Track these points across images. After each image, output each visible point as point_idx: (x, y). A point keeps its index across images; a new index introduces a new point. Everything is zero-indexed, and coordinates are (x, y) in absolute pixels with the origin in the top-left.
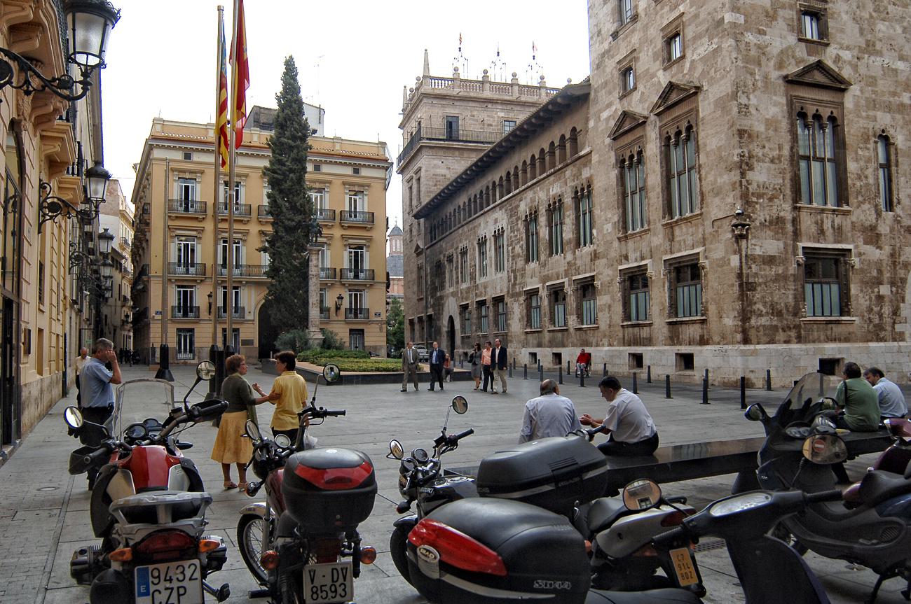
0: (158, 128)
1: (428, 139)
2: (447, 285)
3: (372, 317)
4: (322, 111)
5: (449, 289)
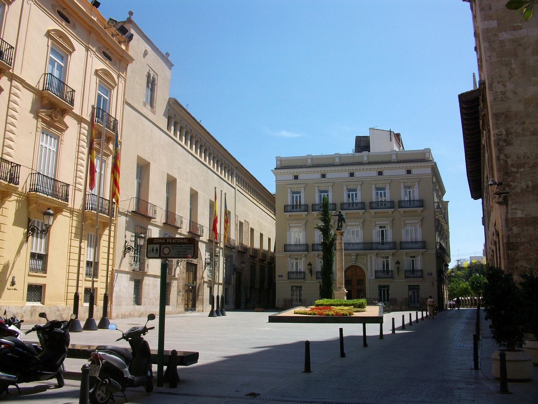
4: (392, 133)
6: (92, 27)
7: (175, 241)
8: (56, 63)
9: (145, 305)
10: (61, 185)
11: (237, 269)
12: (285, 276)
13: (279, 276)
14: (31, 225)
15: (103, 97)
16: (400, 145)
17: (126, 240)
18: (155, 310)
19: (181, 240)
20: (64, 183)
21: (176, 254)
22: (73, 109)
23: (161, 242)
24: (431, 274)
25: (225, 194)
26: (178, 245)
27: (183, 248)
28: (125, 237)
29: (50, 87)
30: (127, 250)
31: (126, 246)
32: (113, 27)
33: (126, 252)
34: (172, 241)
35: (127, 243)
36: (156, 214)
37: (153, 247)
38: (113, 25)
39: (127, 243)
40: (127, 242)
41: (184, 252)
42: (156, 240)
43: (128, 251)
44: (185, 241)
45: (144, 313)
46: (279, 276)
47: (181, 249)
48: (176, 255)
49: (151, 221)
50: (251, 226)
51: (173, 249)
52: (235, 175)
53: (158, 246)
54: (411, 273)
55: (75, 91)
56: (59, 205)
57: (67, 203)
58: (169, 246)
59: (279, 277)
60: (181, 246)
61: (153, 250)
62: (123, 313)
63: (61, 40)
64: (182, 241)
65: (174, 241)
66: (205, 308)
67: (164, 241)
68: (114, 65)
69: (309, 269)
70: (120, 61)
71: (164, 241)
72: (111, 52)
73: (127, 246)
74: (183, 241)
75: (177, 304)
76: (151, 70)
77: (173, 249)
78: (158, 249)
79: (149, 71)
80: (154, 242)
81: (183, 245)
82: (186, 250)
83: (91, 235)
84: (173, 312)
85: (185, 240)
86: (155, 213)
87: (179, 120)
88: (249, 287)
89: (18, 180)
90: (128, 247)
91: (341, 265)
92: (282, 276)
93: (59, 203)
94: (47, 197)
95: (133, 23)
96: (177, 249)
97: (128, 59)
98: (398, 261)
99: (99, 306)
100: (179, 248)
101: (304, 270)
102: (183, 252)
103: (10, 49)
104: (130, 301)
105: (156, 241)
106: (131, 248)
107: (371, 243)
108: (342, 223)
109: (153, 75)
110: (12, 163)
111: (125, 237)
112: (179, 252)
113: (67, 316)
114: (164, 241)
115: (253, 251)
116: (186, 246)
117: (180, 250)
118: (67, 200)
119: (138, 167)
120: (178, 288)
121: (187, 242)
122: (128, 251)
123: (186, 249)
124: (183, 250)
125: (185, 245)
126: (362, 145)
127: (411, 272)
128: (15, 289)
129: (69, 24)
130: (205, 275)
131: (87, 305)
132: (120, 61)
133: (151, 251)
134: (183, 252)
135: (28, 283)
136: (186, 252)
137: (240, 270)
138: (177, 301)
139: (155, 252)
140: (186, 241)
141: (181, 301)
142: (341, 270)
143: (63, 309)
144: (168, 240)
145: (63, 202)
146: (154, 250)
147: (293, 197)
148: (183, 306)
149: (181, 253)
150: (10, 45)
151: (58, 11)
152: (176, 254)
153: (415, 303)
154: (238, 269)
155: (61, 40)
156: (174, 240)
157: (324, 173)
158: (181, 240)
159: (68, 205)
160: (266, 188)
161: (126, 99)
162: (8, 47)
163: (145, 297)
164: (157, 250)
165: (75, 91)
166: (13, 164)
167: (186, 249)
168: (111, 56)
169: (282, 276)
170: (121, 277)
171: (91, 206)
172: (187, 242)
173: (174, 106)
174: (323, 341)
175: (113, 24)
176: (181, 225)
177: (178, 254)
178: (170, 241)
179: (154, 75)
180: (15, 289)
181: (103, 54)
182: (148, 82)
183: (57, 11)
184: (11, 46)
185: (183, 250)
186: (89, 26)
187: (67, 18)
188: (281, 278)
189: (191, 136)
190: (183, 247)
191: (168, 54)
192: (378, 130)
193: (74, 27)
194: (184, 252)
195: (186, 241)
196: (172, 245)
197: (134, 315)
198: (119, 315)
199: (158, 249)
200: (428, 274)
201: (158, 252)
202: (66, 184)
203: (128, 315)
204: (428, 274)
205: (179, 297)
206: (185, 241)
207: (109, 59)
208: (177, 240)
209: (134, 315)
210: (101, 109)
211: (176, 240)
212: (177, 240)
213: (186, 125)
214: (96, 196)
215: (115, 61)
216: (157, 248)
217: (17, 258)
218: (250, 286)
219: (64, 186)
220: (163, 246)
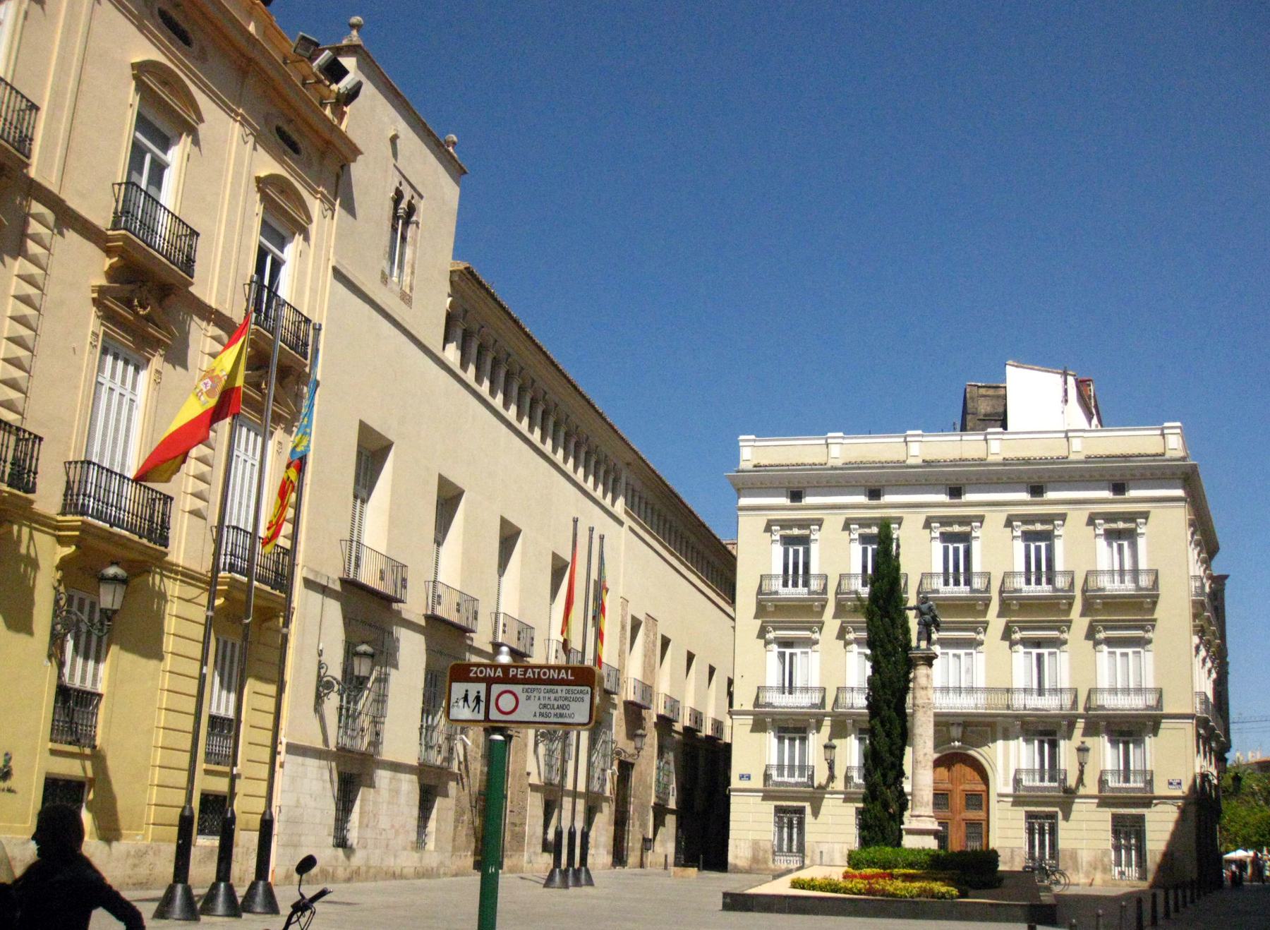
3: (1160, 789)
6: (250, 60)
7: (534, 673)
8: (148, 158)
9: (365, 847)
10: (150, 496)
12: (757, 782)
13: (742, 777)
15: (274, 253)
16: (1091, 413)
17: (320, 661)
18: (392, 865)
19: (552, 671)
20: (157, 492)
21: (538, 715)
22: (191, 284)
23: (492, 675)
24: (1179, 784)
25: (602, 538)
26: (543, 687)
27: (560, 694)
29: (132, 219)
32: (306, 60)
34: (525, 674)
36: (405, 587)
37: (467, 691)
38: (308, 54)
41: (561, 707)
42: (475, 669)
44: (565, 676)
45: (363, 869)
46: (742, 777)
47: (552, 698)
48: (535, 716)
50: (662, 629)
51: (528, 698)
52: (623, 486)
53: (482, 687)
54: (1121, 779)
55: (198, 235)
56: (141, 553)
57: (162, 548)
58: (517, 689)
60: (551, 691)
61: (466, 699)
63: (167, 93)
64: (556, 676)
65: (529, 674)
66: (530, 862)
67: (499, 673)
68: (307, 166)
69: (826, 760)
70: (323, 155)
71: (501, 675)
72: (298, 130)
74: (495, 673)
75: (454, 847)
76: (404, 183)
77: (528, 698)
78: (483, 697)
79: (398, 185)
80: (471, 675)
81: (559, 688)
82: (566, 703)
83: (233, 645)
84: (442, 871)
85: (563, 671)
86: (404, 586)
87: (477, 327)
88: (652, 804)
89: (34, 478)
92: (749, 777)
93: (141, 547)
94: (111, 530)
95: (361, 51)
96: (539, 699)
97: (344, 149)
100: (547, 695)
102: (558, 708)
103: (28, 112)
104: (326, 834)
105: (476, 673)
106: (335, 682)
107: (1008, 690)
109: (410, 198)
110: (18, 429)
112: (545, 706)
113: (148, 872)
114: (499, 673)
115: (668, 704)
116: (568, 691)
117: (547, 702)
118: (164, 541)
119: (359, 454)
121: (569, 677)
123: (566, 699)
124: (556, 704)
125: (564, 688)
126: (983, 411)
127: (1122, 774)
128: (10, 790)
129: (187, 47)
130: (531, 766)
131: (214, 842)
132: (323, 155)
133: (461, 703)
134: (558, 708)
135: (47, 773)
136: (567, 707)
137: (630, 756)
138: (454, 840)
139: (472, 704)
140: (567, 676)
141: (464, 838)
143: (140, 850)
144: (511, 670)
145: (151, 545)
146: (471, 698)
147: (946, 550)
148: (469, 853)
149: (553, 711)
150: (28, 101)
151: (159, 9)
152: (538, 715)
153: (1131, 866)
154: (625, 752)
155: (167, 93)
156: (530, 670)
157: (1040, 482)
158: (552, 671)
159: (166, 554)
160: (707, 525)
162: (23, 107)
163: (367, 826)
164: (478, 699)
165: (198, 235)
166: (21, 434)
167: (566, 699)
168: (298, 141)
169: (749, 777)
170: (303, 765)
171: (228, 561)
172: (569, 677)
173: (463, 284)
175: (308, 52)
176: (474, 621)
177: (541, 715)
178: (519, 673)
179: (413, 198)
180: (10, 790)
181: (276, 135)
182: (396, 217)
183: (157, 9)
184: (29, 104)
185: (556, 704)
186: (243, 55)
187: (184, 31)
189: (508, 371)
190: (557, 692)
192: (598, 417)
193: (201, 58)
194: (561, 707)
195: (567, 676)
196: (527, 686)
197: (333, 876)
199: (483, 697)
200: (1171, 784)
201: (482, 705)
202: (164, 495)
203: (317, 876)
205: (460, 828)
206: (563, 675)
207: (294, 148)
208: (539, 673)
209: (333, 876)
210: (265, 286)
211: (537, 670)
212: (539, 673)
213: (496, 341)
214: (250, 534)
215: (309, 154)
216: (478, 692)
217: (808, 828)
218: (655, 804)
219: (157, 502)
220: (496, 689)
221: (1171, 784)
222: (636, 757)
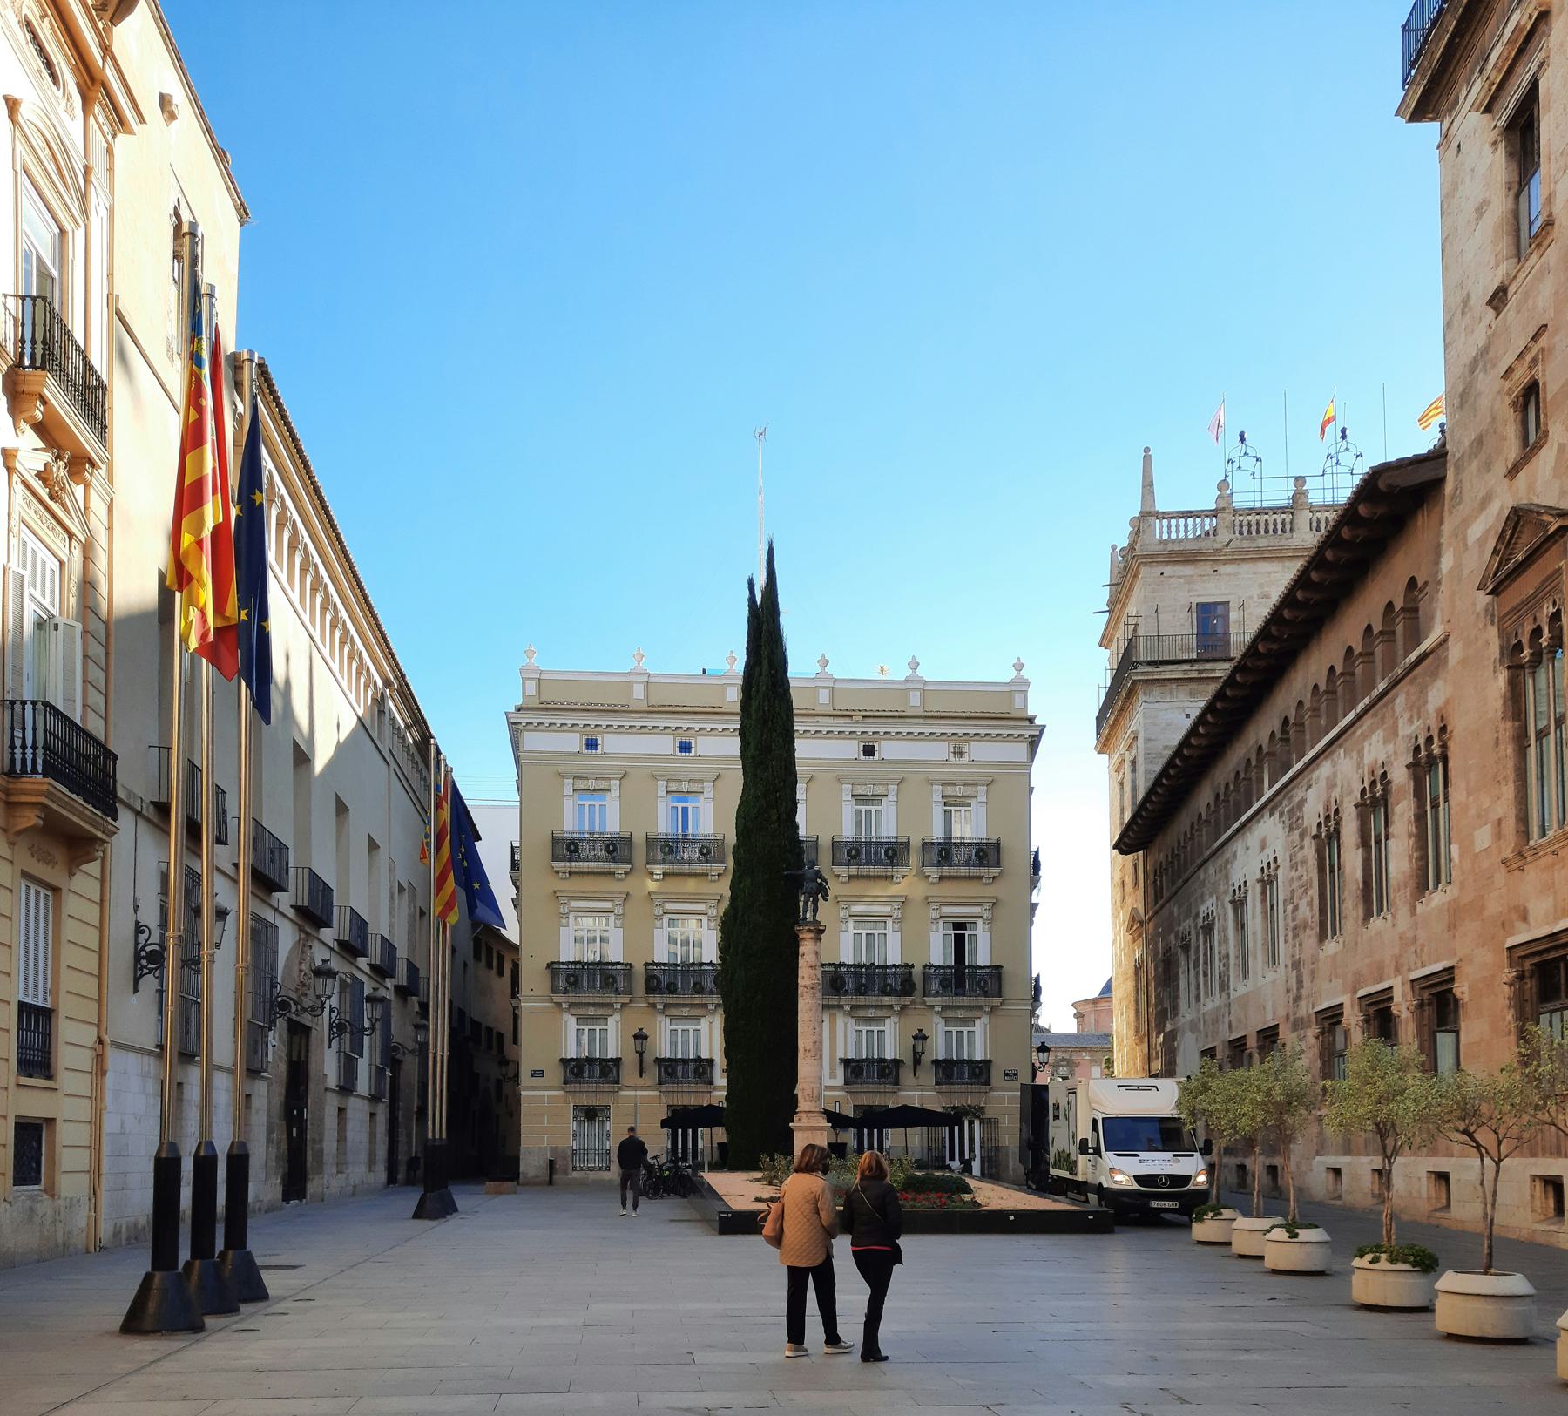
0: (532, 688)
1: (1150, 663)
2: (1183, 1004)
5: (1186, 1014)
11: (401, 1050)
13: (535, 1074)
14: (147, 941)
17: (137, 922)
24: (1016, 1074)
28: (136, 908)
30: (144, 962)
31: (140, 946)
33: (139, 972)
35: (146, 935)
39: (146, 935)
40: (143, 932)
43: (150, 966)
46: (535, 1074)
49: (43, 816)
59: (532, 1076)
62: (133, 1219)
73: (145, 945)
88: (415, 1109)
90: (148, 949)
91: (815, 1038)
98: (920, 1030)
99: (63, 1195)
101: (617, 1053)
108: (815, 903)
111: (136, 908)
120: (269, 1116)
122: (150, 966)
142: (815, 1056)
161: (117, 302)
169: (541, 1073)
174: (1026, 1233)
188: (537, 1081)
191: (1345, 918)
198: (120, 1232)
204: (1006, 1075)
221: (1006, 1075)
222: (319, 1012)
